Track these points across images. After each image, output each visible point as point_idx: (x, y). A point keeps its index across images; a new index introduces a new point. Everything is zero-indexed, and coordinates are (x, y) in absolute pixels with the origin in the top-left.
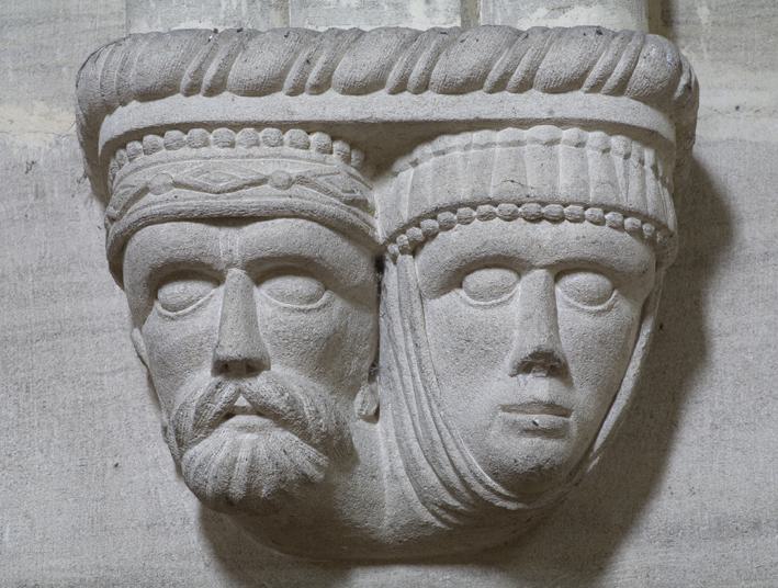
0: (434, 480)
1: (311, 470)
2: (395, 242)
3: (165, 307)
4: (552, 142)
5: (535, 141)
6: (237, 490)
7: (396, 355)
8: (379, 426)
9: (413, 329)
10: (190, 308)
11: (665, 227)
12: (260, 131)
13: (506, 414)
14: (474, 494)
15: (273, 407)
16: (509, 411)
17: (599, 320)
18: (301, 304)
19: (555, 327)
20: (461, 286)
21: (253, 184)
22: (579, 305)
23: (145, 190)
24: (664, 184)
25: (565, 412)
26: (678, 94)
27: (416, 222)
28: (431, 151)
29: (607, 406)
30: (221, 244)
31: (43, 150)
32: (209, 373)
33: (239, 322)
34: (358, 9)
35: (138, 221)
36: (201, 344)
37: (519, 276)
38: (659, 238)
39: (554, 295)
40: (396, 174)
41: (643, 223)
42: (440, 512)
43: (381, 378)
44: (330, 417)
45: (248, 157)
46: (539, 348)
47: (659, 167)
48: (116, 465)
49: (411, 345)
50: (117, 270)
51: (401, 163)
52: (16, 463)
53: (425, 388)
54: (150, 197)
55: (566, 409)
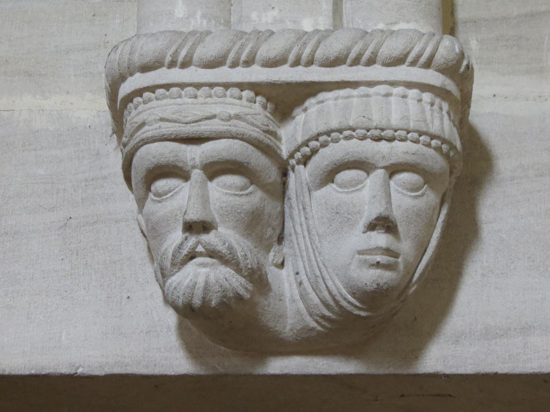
0: (317, 301)
1: (242, 292)
2: (293, 158)
3: (155, 195)
4: (388, 95)
5: (378, 94)
6: (197, 302)
7: (294, 227)
8: (284, 272)
9: (304, 209)
10: (170, 194)
11: (455, 147)
12: (212, 89)
13: (361, 256)
14: (341, 307)
15: (219, 252)
16: (363, 254)
17: (416, 201)
18: (236, 191)
19: (389, 202)
20: (333, 182)
21: (208, 118)
22: (405, 192)
23: (143, 124)
24: (454, 125)
25: (396, 255)
26: (462, 69)
27: (306, 144)
28: (315, 102)
29: (420, 258)
30: (188, 155)
31: (89, 120)
32: (181, 233)
33: (199, 199)
34: (272, 24)
35: (139, 142)
36: (176, 216)
37: (368, 174)
38: (452, 154)
39: (389, 185)
40: (294, 118)
41: (442, 144)
42: (320, 320)
43: (286, 242)
44: (254, 259)
45: (205, 103)
46: (380, 214)
47: (452, 114)
48: (128, 297)
49: (303, 219)
50: (128, 179)
51: (297, 111)
52: (70, 296)
53: (311, 243)
54: (146, 128)
55: (397, 253)
